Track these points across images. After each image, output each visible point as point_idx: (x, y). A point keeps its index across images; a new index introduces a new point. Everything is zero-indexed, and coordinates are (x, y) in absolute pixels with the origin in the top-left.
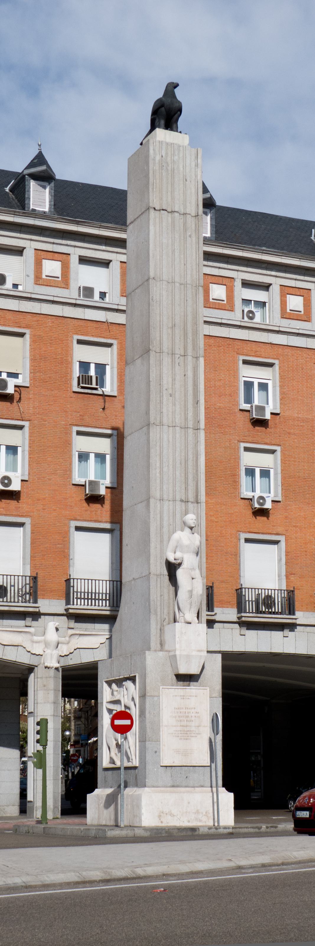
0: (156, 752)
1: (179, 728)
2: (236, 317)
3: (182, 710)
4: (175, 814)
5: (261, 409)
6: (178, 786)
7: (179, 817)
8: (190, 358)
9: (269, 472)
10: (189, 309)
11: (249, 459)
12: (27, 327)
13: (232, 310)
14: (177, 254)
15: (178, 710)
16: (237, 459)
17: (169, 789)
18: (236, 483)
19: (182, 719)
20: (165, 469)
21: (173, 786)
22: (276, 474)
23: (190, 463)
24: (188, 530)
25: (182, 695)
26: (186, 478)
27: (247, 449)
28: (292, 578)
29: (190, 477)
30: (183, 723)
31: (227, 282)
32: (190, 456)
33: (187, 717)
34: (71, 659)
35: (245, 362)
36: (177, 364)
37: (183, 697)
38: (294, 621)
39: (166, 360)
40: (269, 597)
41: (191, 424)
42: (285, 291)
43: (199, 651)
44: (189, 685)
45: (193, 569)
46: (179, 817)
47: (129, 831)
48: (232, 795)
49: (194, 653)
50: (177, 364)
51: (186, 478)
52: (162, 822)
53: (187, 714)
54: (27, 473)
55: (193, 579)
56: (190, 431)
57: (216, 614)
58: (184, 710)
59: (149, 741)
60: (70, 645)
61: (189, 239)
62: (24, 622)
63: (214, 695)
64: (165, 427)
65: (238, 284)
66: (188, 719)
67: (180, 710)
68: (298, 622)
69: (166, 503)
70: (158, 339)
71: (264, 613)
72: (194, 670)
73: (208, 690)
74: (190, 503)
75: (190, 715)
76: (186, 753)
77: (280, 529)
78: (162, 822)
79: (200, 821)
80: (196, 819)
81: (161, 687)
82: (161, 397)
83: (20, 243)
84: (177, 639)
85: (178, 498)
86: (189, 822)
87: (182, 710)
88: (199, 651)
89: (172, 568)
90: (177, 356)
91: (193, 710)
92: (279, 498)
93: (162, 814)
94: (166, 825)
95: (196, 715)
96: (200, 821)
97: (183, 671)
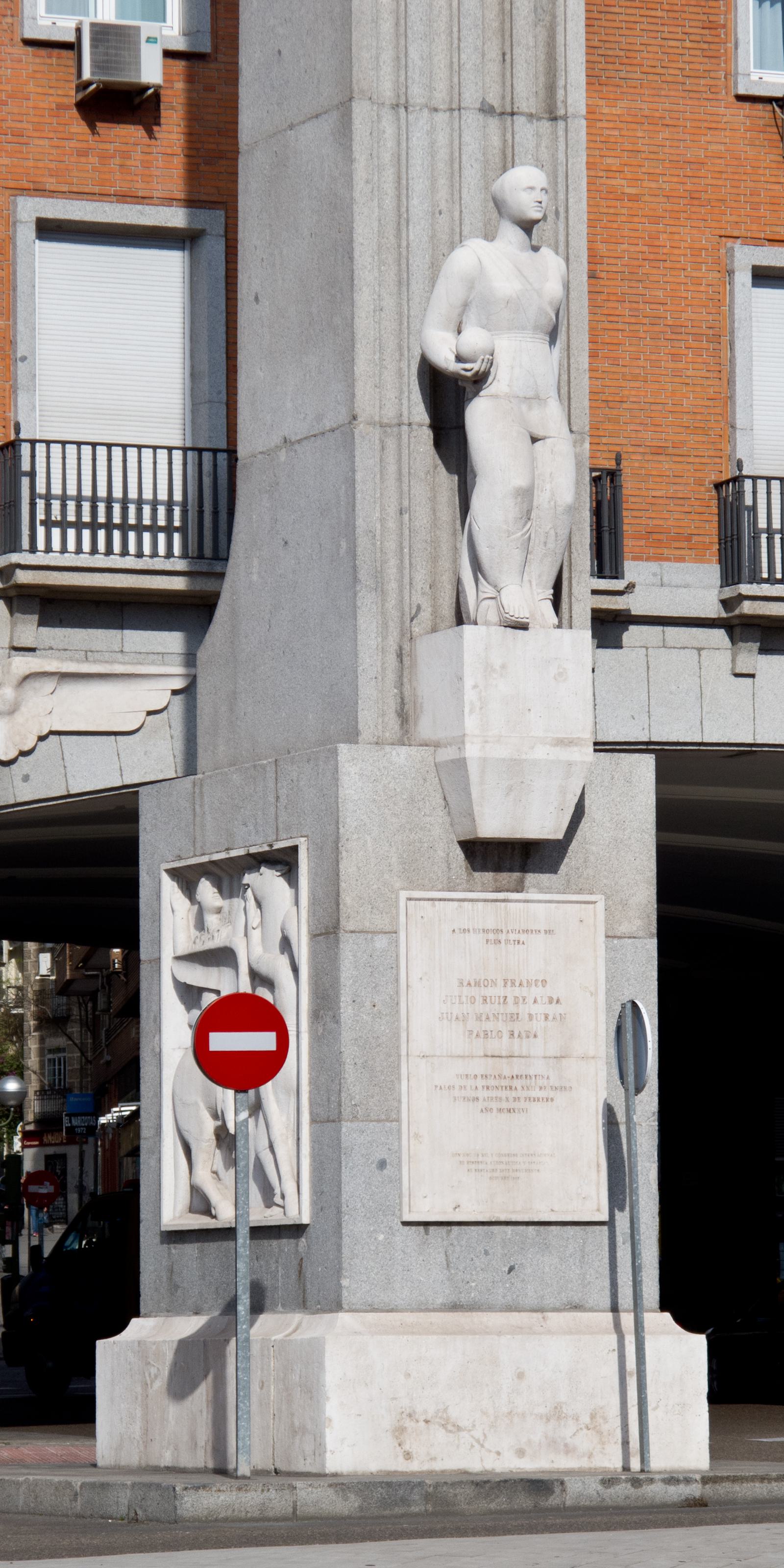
0: (382, 1164)
1: (478, 1066)
3: (490, 992)
7: (478, 1434)
15: (474, 991)
19: (489, 1026)
21: (455, 1307)
24: (512, 234)
25: (490, 925)
33: (514, 1017)
34: (26, 778)
37: (495, 936)
44: (519, 888)
46: (478, 1434)
49: (541, 753)
52: (408, 1456)
53: (511, 1008)
55: (534, 440)
57: (631, 587)
59: (355, 1118)
60: (19, 718)
66: (517, 1027)
69: (420, 122)
72: (541, 823)
73: (601, 906)
74: (520, 120)
75: (523, 1010)
76: (507, 1170)
78: (408, 1456)
79: (568, 1450)
80: (552, 1443)
81: (403, 895)
85: (471, 97)
86: (521, 1453)
87: (490, 992)
89: (447, 395)
91: (537, 991)
93: (408, 1423)
94: (426, 1467)
95: (552, 1009)
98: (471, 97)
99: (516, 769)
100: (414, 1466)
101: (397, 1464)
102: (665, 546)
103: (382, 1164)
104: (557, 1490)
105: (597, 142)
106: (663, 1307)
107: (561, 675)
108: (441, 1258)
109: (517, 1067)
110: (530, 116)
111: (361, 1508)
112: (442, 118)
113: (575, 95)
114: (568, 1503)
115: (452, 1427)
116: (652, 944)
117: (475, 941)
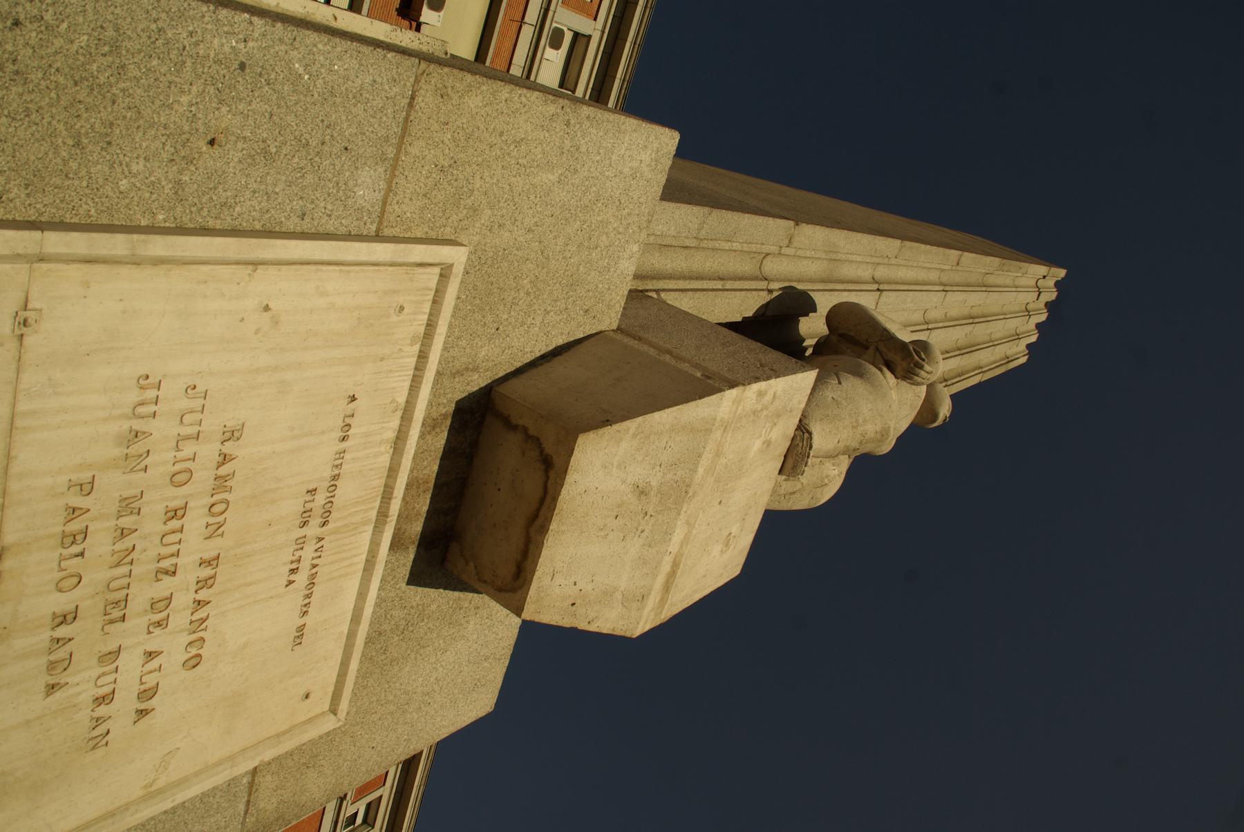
15: (204, 476)
19: (101, 544)
37: (318, 511)
53: (141, 595)
58: (194, 546)
75: (133, 636)
87: (195, 522)
95: (126, 702)
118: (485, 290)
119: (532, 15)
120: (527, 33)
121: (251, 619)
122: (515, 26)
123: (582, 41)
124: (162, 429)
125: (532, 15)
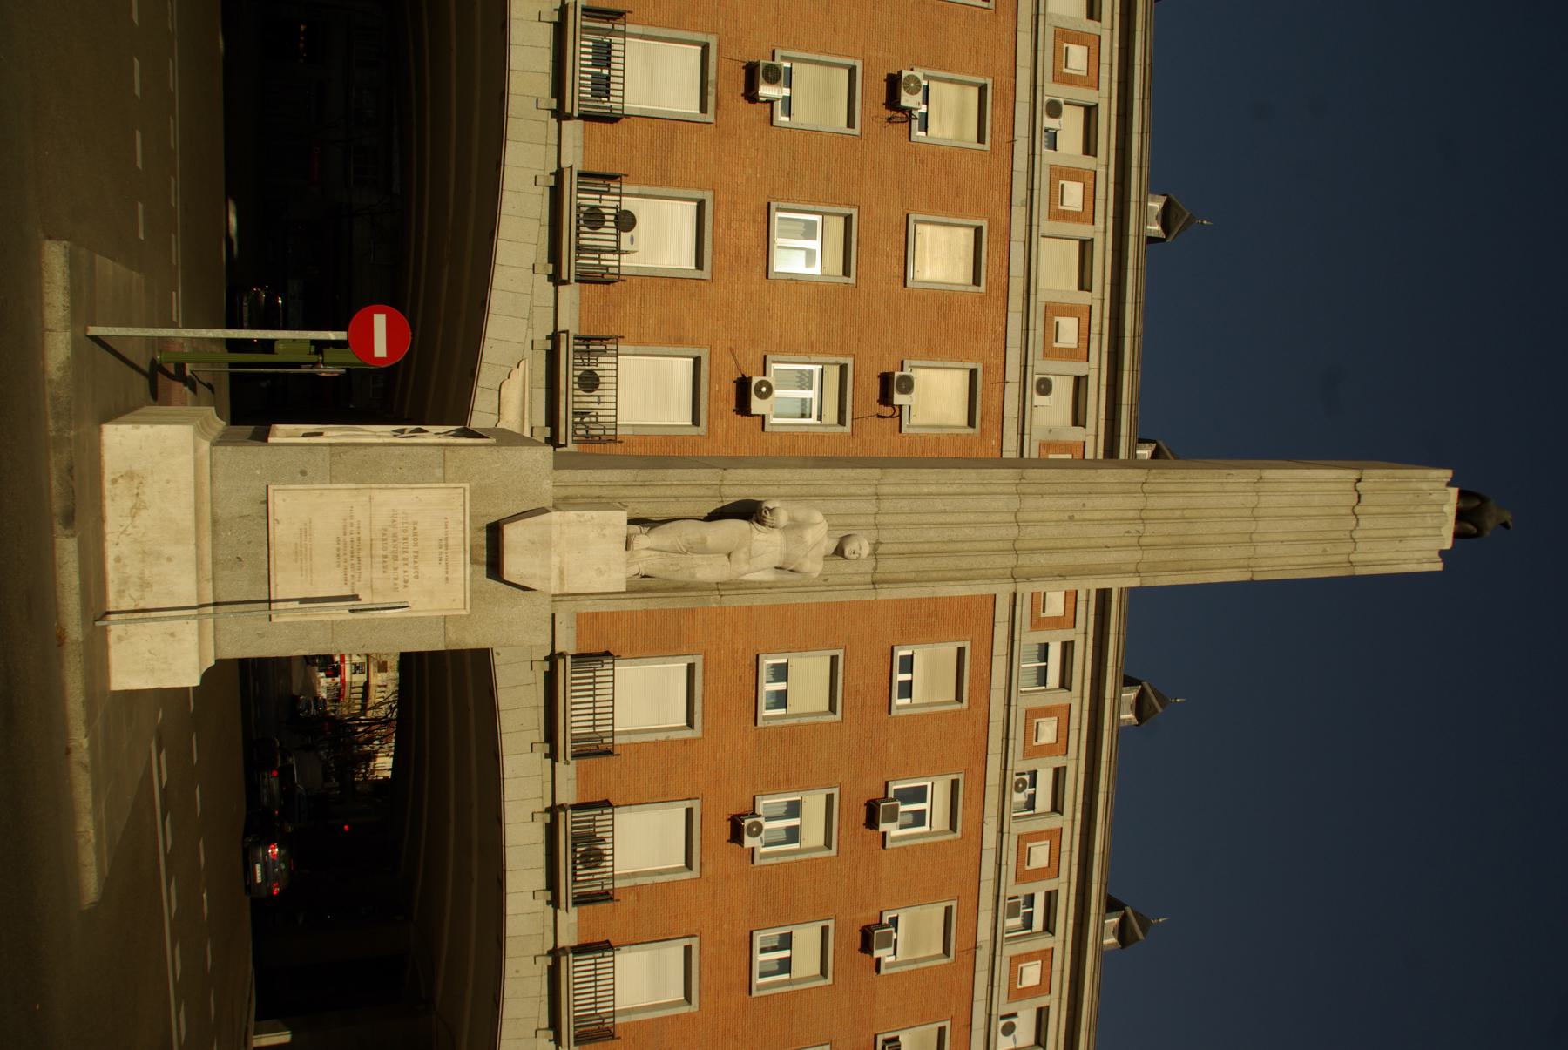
0: (303, 473)
1: (365, 535)
2: (1019, 764)
3: (410, 542)
4: (137, 521)
5: (892, 816)
6: (215, 534)
7: (130, 530)
8: (1138, 555)
9: (795, 841)
10: (1215, 553)
11: (814, 804)
12: (982, 431)
13: (1026, 755)
14: (1299, 525)
15: (410, 532)
16: (812, 787)
17: (207, 507)
18: (776, 787)
19: (390, 541)
20: (939, 504)
21: (215, 522)
22: (794, 852)
23: (950, 562)
24: (833, 545)
25: (451, 542)
26: (921, 554)
27: (829, 798)
28: (632, 898)
29: (925, 563)
30: (378, 544)
31: (1061, 745)
32: (964, 563)
33: (395, 558)
35: (955, 783)
36: (1128, 528)
37: (444, 545)
38: (563, 905)
39: (1135, 502)
40: (600, 857)
41: (1025, 560)
42: (1055, 836)
43: (562, 572)
44: (473, 561)
45: (751, 557)
46: (130, 530)
47: (61, 313)
48: (195, 681)
49: (555, 560)
50: (1128, 528)
51: (921, 554)
52: (114, 481)
53: (401, 556)
54: (775, 429)
55: (729, 555)
56: (1010, 561)
57: (567, 763)
58: (411, 548)
59: (332, 455)
61: (1319, 548)
62: (543, 423)
63: (450, 627)
64: (1014, 504)
65: (1059, 761)
66: (389, 560)
67: (411, 538)
68: (561, 913)
69: (871, 507)
70: (1165, 488)
71: (574, 851)
72: (513, 566)
73: (463, 613)
74: (873, 562)
75: (400, 563)
76: (301, 554)
77: (709, 868)
78: (114, 481)
79: (121, 592)
80: (125, 581)
81: (467, 485)
82: (1070, 494)
83: (1091, 421)
84: (588, 514)
85: (885, 535)
86: (118, 560)
87: (410, 542)
88: (562, 572)
89: (749, 511)
90: (1141, 528)
91: (411, 573)
92: (758, 861)
93: (136, 481)
94: (107, 494)
95: (400, 583)
96: (121, 592)
97: (513, 534)
98: (885, 535)
99: (545, 545)
100: (107, 485)
101: (108, 476)
102: (582, 779)
103: (303, 473)
104: (67, 532)
105: (865, 607)
106: (217, 661)
107: (600, 572)
108: (245, 512)
109: (365, 560)
110: (875, 568)
111: (51, 381)
112: (871, 519)
113: (886, 594)
114: (58, 541)
115: (134, 512)
116: (441, 647)
117: (441, 532)
118: (477, 495)
119: (1013, 373)
120: (1012, 391)
121: (432, 571)
122: (999, 387)
123: (1083, 381)
124: (399, 520)
125: (1013, 373)
